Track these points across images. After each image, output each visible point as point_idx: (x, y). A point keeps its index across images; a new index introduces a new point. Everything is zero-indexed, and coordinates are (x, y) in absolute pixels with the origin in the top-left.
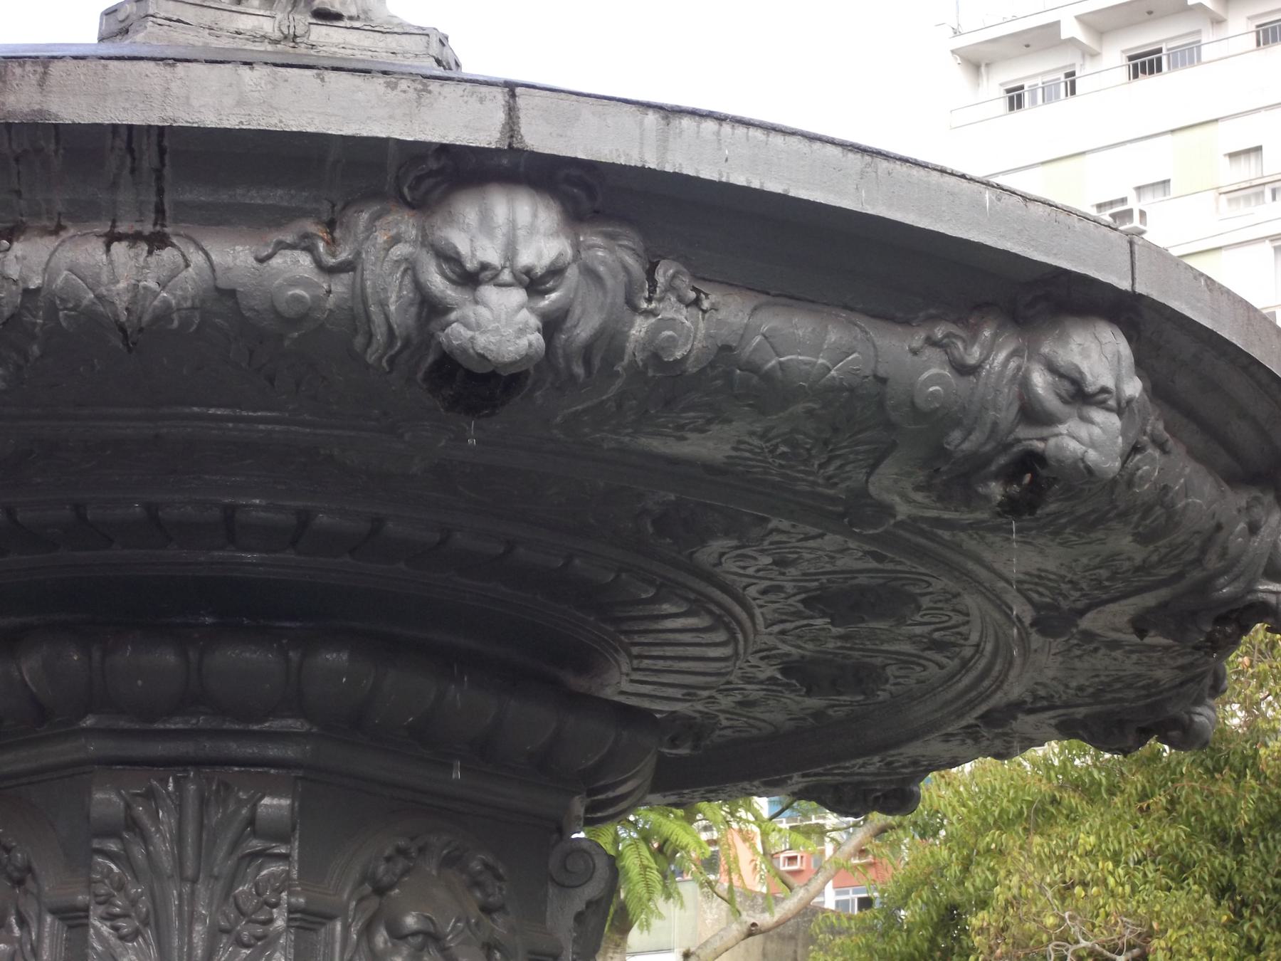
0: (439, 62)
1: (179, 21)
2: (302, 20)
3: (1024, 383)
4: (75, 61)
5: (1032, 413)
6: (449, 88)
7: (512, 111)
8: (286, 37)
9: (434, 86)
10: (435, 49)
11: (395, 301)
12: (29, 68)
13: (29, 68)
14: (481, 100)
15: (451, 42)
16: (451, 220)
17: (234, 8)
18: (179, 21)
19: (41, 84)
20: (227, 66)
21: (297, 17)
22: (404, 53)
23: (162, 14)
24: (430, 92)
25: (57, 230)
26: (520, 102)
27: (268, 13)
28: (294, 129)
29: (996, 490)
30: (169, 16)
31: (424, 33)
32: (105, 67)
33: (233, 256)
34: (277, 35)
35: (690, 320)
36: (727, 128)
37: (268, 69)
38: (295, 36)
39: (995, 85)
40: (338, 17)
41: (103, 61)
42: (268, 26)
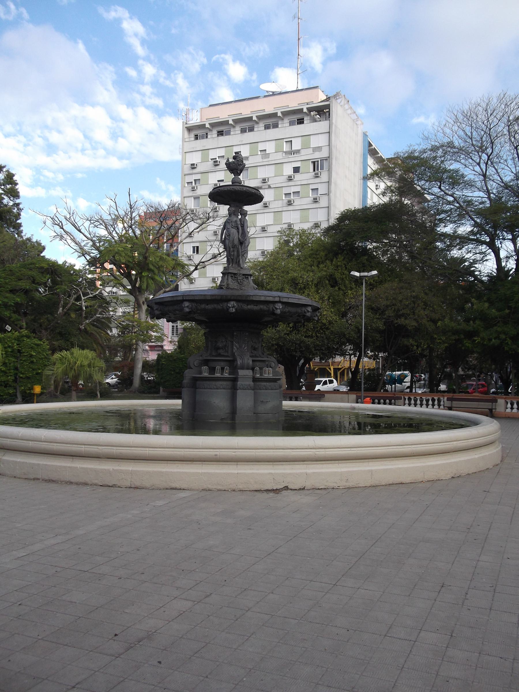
5: (305, 312)
11: (271, 310)
39: (192, 135)
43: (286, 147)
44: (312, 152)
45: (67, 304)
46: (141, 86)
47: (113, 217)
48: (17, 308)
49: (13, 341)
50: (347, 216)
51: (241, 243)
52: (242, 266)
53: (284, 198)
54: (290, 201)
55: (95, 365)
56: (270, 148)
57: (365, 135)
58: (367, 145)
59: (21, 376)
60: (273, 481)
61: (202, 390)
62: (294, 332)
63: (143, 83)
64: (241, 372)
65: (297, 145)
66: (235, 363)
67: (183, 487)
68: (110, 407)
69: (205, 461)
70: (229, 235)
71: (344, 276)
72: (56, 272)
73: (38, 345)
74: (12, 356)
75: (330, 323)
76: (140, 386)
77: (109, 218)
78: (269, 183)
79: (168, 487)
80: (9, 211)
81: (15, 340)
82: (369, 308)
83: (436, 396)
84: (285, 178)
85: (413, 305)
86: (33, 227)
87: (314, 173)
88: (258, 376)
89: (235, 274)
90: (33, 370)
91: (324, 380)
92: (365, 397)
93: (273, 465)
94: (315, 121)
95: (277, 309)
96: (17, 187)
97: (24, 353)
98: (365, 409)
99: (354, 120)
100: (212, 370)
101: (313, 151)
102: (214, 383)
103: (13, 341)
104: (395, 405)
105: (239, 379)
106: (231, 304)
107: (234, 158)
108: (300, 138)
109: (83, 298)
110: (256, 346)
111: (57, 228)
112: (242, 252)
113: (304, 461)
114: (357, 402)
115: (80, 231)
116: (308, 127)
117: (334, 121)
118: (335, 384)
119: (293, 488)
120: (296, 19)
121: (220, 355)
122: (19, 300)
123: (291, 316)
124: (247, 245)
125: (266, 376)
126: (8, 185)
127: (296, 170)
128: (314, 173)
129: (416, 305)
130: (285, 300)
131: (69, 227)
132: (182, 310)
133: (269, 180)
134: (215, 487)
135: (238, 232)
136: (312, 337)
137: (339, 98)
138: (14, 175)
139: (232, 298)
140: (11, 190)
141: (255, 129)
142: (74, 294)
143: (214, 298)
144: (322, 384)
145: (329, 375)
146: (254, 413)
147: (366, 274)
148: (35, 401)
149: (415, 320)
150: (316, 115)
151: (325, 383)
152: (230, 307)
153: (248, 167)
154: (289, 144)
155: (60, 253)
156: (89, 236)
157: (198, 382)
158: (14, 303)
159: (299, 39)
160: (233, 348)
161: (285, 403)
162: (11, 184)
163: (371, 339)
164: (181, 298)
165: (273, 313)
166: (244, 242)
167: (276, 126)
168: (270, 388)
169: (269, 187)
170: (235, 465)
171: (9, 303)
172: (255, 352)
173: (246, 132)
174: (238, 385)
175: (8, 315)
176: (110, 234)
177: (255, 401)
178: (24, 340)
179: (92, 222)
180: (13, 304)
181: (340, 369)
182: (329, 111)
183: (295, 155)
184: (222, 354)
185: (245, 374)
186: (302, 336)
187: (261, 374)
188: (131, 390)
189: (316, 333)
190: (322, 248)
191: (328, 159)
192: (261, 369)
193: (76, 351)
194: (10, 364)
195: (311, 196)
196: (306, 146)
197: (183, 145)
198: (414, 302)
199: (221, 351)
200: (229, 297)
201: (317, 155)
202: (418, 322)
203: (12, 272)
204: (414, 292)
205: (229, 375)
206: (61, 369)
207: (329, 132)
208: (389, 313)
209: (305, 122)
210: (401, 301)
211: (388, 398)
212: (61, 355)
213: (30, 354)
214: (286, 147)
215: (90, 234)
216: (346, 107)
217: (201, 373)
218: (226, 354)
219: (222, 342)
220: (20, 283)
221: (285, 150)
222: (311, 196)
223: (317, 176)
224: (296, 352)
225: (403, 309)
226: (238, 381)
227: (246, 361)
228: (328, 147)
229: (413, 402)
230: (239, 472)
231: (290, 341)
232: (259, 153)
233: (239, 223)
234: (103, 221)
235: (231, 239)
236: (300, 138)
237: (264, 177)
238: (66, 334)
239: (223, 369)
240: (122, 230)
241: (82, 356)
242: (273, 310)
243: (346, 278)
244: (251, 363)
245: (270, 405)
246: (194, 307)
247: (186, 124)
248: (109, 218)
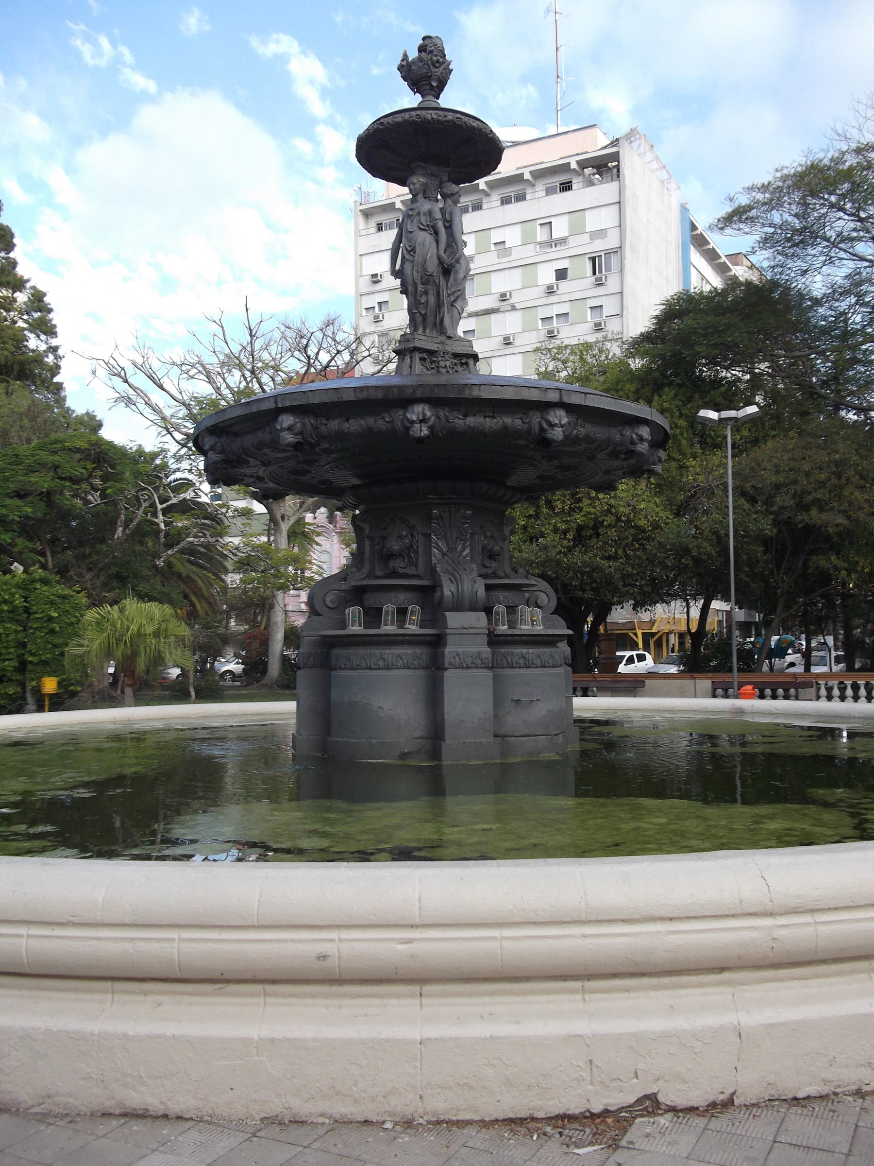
3: (632, 436)
5: (633, 442)
11: (536, 428)
16: (548, 414)
25: (475, 415)
29: (623, 456)
33: (508, 420)
35: (583, 430)
39: (373, 224)
43: (541, 235)
44: (589, 241)
45: (132, 521)
47: (222, 357)
48: (28, 529)
49: (13, 590)
50: (681, 312)
51: (447, 271)
52: (449, 332)
53: (540, 327)
54: (552, 331)
55: (170, 632)
56: (512, 237)
57: (684, 209)
58: (688, 227)
59: (30, 659)
60: (585, 1074)
61: (344, 673)
62: (577, 549)
64: (454, 620)
65: (560, 229)
66: (437, 595)
67: (174, 1108)
68: (151, 724)
69: (274, 982)
70: (412, 250)
71: (678, 431)
72: (105, 459)
73: (64, 597)
74: (12, 620)
75: (656, 526)
76: (280, 675)
77: (215, 360)
78: (512, 301)
79: (109, 1105)
80: (38, 359)
81: (20, 588)
82: (740, 492)
83: (862, 678)
84: (540, 291)
85: (834, 481)
86: (82, 390)
87: (593, 278)
88: (503, 628)
89: (431, 353)
90: (55, 646)
91: (627, 654)
92: (741, 685)
93: (583, 991)
94: (591, 184)
95: (552, 425)
96: (51, 316)
97: (36, 613)
98: (771, 714)
99: (662, 182)
100: (373, 616)
101: (591, 239)
102: (377, 651)
103: (13, 590)
104: (797, 698)
105: (450, 639)
106: (416, 412)
107: (422, 49)
108: (566, 217)
109: (159, 507)
110: (497, 548)
111: (117, 381)
112: (449, 295)
113: (722, 970)
114: (714, 696)
115: (161, 387)
116: (581, 195)
117: (627, 182)
118: (649, 662)
119: (681, 1102)
120: (552, 14)
121: (394, 574)
122: (29, 510)
123: (591, 458)
124: (461, 276)
125: (525, 628)
126: (36, 312)
127: (561, 274)
128: (593, 278)
129: (843, 481)
130: (575, 400)
131: (140, 380)
132: (275, 444)
133: (513, 295)
134: (321, 1106)
135: (437, 241)
136: (615, 558)
137: (635, 140)
138: (44, 295)
139: (419, 394)
140: (39, 322)
141: (485, 206)
142: (145, 500)
143: (364, 395)
144: (624, 662)
145: (634, 646)
146: (495, 736)
147: (732, 413)
148: (47, 708)
149: (844, 512)
150: (594, 174)
151: (630, 660)
152: (413, 422)
153: (473, 275)
154: (547, 227)
155: (127, 430)
156: (179, 396)
157: (335, 651)
158: (20, 517)
159: (557, 49)
160: (429, 554)
161: (579, 702)
162: (40, 311)
163: (745, 557)
164: (272, 405)
165: (544, 442)
166: (452, 266)
167: (521, 198)
168: (538, 663)
169: (514, 308)
170: (412, 996)
171: (10, 518)
172: (494, 564)
173: (468, 211)
174: (446, 654)
175: (9, 541)
176: (218, 389)
177: (498, 700)
178: (36, 589)
179: (184, 368)
180: (18, 519)
181: (653, 635)
182: (618, 165)
183: (558, 248)
184: (401, 571)
185: (466, 624)
186: (595, 556)
187: (512, 625)
188: (264, 682)
189: (624, 551)
190: (629, 377)
191: (619, 251)
192: (511, 609)
193: (131, 605)
194: (7, 635)
195: (589, 320)
196: (577, 229)
197: (356, 242)
198: (839, 476)
199: (398, 564)
200: (410, 391)
201: (599, 246)
202: (849, 518)
203: (17, 459)
204: (837, 452)
205: (420, 627)
206: (98, 641)
207: (619, 202)
208: (783, 500)
209: (574, 187)
210: (808, 475)
211: (769, 685)
212: (99, 614)
213: (47, 615)
214: (541, 235)
215: (181, 393)
216: (649, 156)
217: (344, 626)
218: (411, 571)
219: (400, 537)
220: (33, 478)
221: (539, 240)
222: (589, 320)
223: (599, 284)
224: (584, 591)
225: (815, 490)
226: (445, 645)
227: (467, 586)
228: (617, 230)
229: (849, 692)
230: (432, 1032)
231: (569, 569)
232: (493, 247)
233: (438, 216)
234: (204, 368)
235: (418, 258)
236: (567, 216)
237: (502, 290)
238: (128, 577)
239: (402, 612)
240: (240, 383)
241: (140, 615)
242: (542, 430)
243: (682, 434)
244: (481, 592)
245: (540, 711)
246: (309, 427)
247: (361, 204)
248: (215, 360)
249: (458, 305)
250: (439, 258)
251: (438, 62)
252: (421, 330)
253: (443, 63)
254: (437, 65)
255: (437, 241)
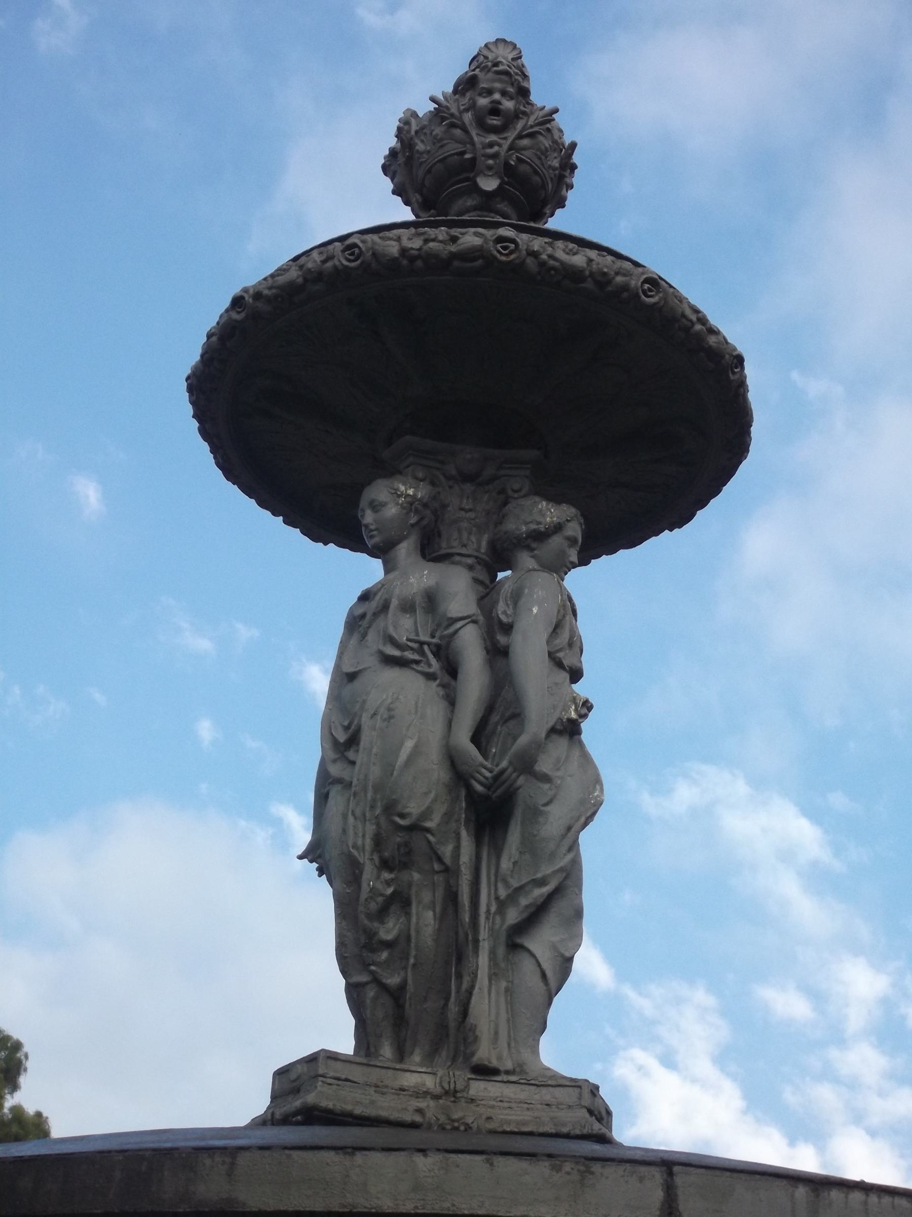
0: (591, 1112)
1: (347, 1080)
2: (461, 1076)
4: (260, 1152)
6: (611, 1171)
7: (670, 1189)
8: (447, 1093)
9: (597, 1168)
10: (587, 1100)
12: (218, 1159)
13: (218, 1159)
14: (641, 1179)
15: (602, 1092)
17: (398, 1066)
18: (347, 1080)
19: (229, 1174)
20: (402, 1153)
21: (457, 1073)
22: (558, 1105)
23: (332, 1074)
24: (592, 1173)
26: (679, 1180)
27: (429, 1070)
28: (466, 1212)
30: (338, 1075)
31: (576, 1084)
32: (289, 1156)
34: (438, 1090)
36: (873, 1198)
37: (439, 1157)
38: (456, 1091)
40: (495, 1072)
41: (287, 1152)
42: (430, 1082)
46: (834, 1053)
51: (492, 810)
63: (840, 1040)
249: (540, 943)
250: (452, 759)
251: (495, 110)
252: (387, 1051)
253: (517, 115)
254: (495, 121)
255: (451, 701)
